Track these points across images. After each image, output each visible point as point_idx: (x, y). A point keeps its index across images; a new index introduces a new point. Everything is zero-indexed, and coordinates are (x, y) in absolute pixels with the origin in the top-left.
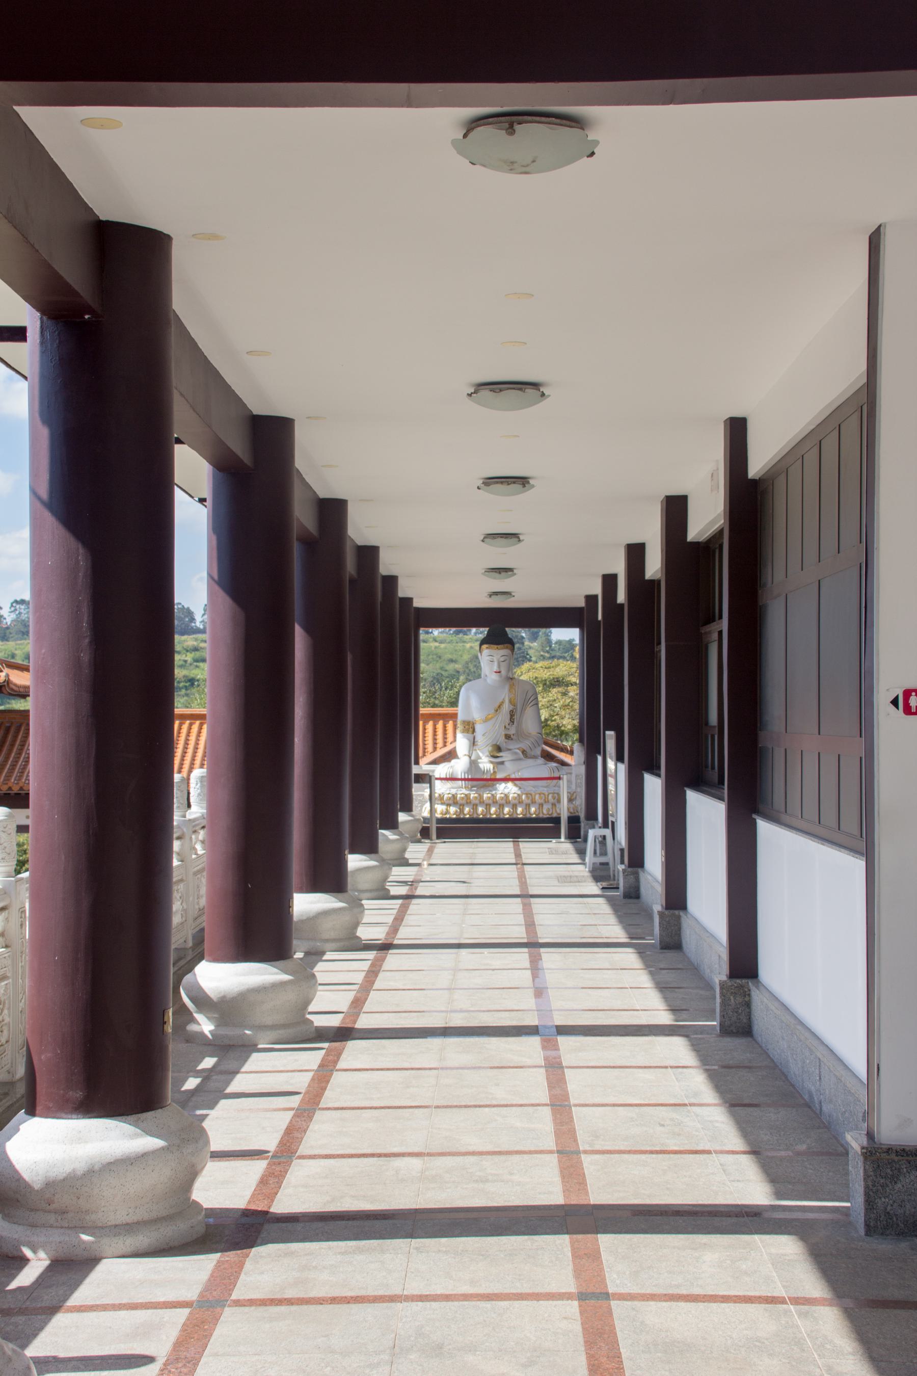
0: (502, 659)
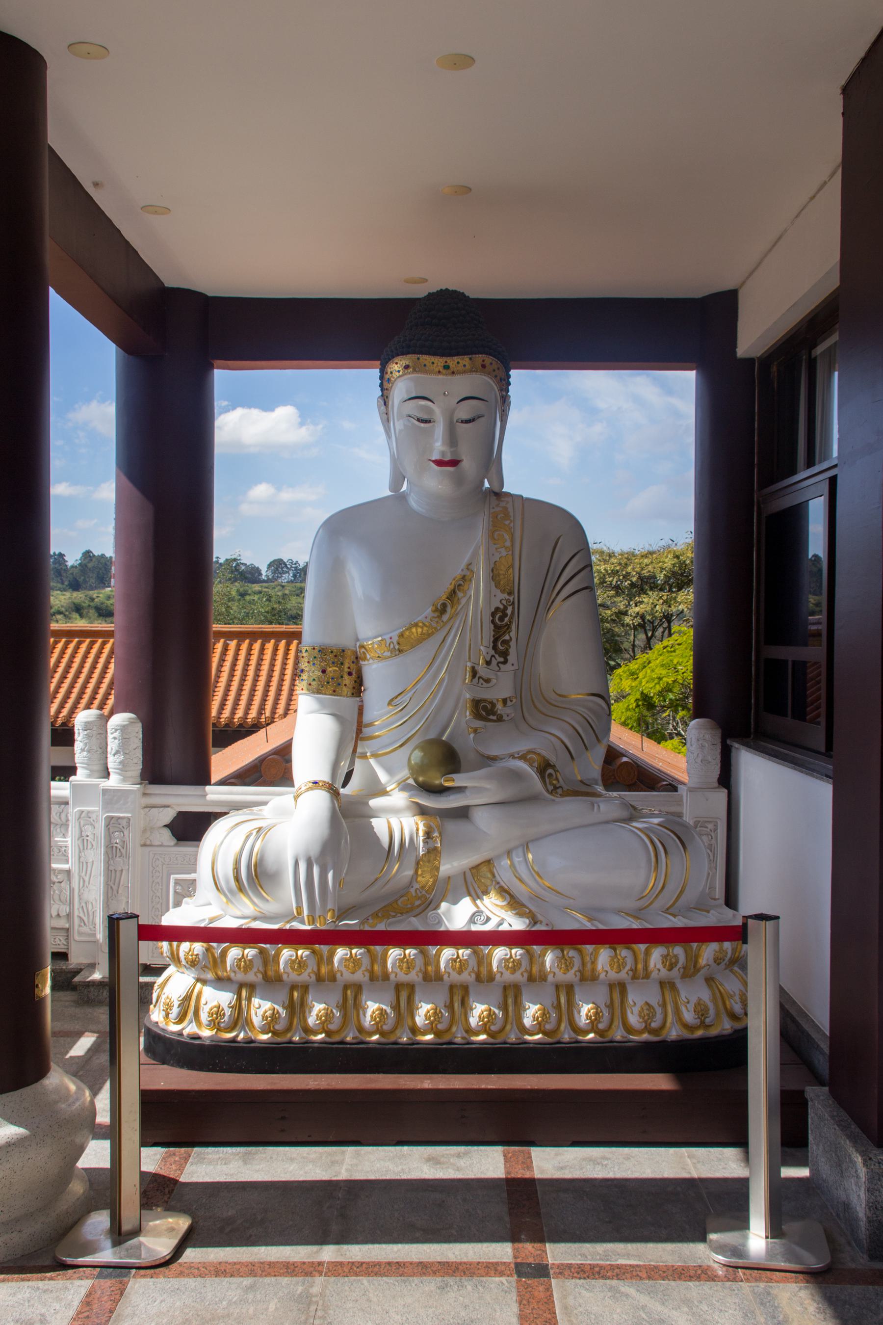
0: (464, 411)
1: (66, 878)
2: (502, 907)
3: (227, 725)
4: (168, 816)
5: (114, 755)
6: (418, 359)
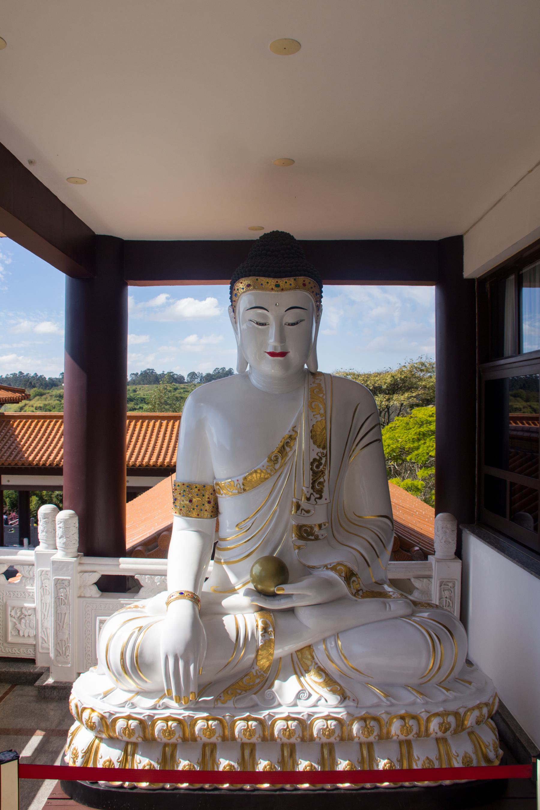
0: (290, 317)
1: (33, 613)
2: (320, 684)
3: (161, 466)
4: (96, 577)
5: (60, 538)
6: (257, 280)
